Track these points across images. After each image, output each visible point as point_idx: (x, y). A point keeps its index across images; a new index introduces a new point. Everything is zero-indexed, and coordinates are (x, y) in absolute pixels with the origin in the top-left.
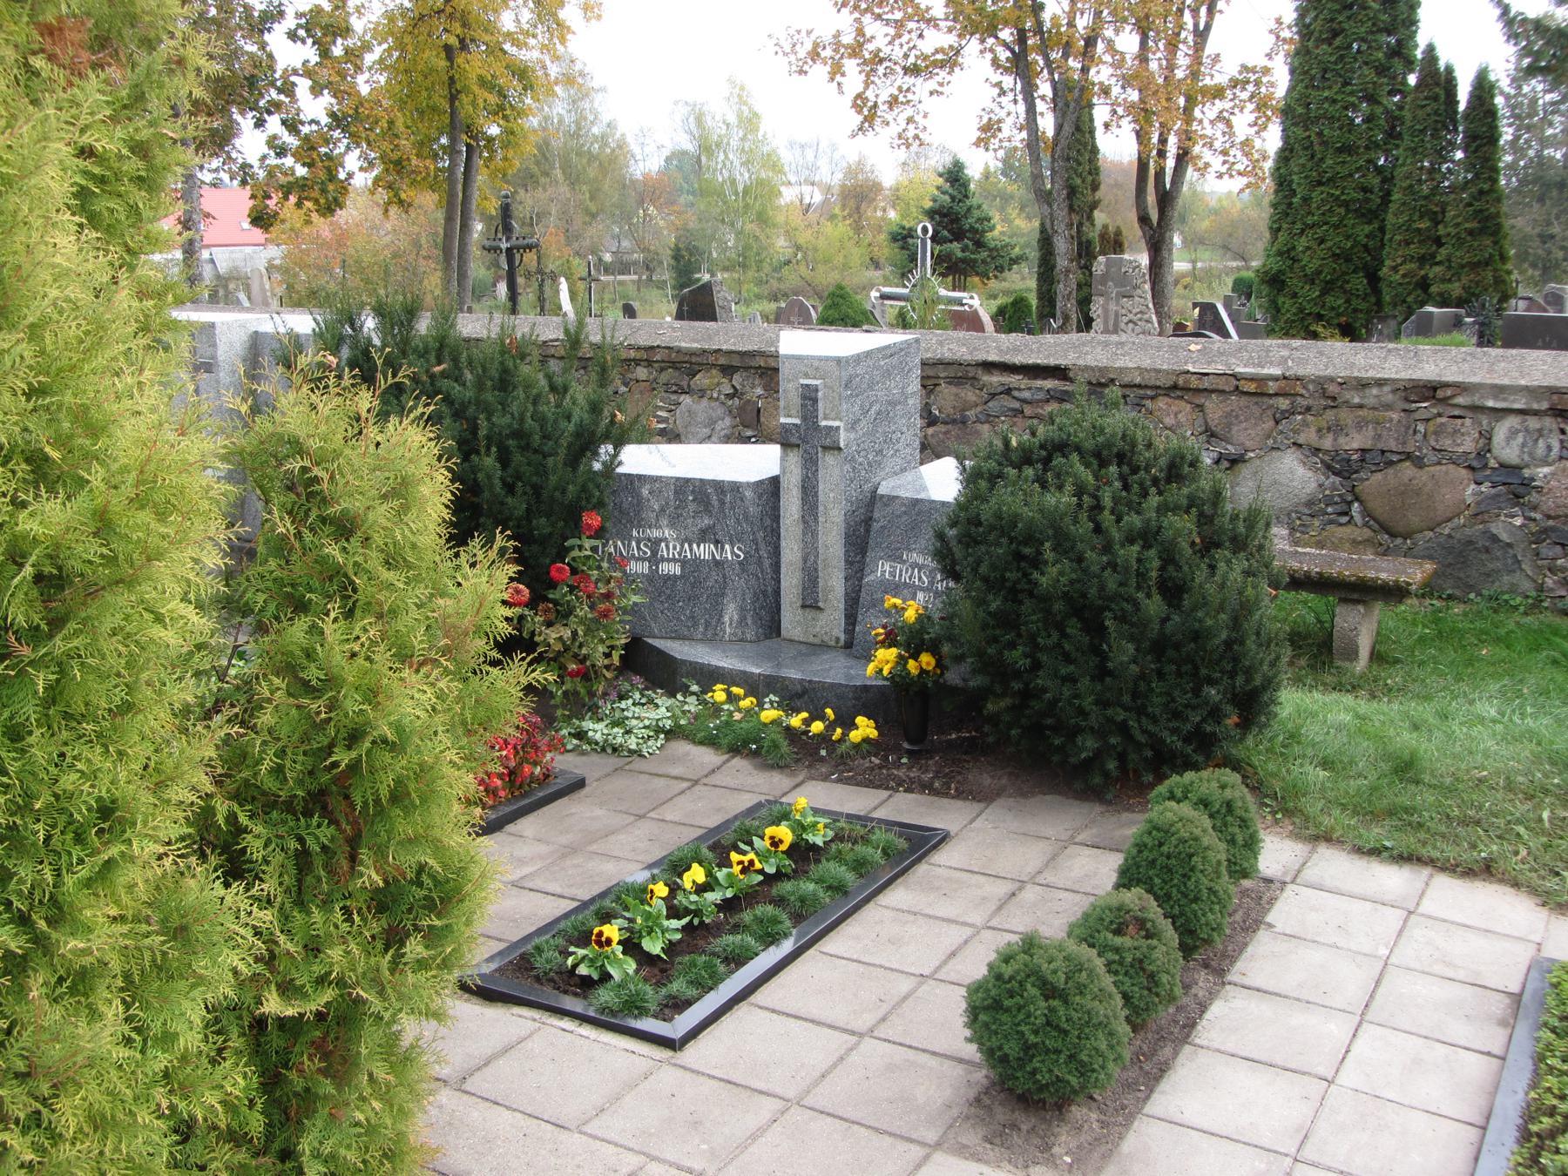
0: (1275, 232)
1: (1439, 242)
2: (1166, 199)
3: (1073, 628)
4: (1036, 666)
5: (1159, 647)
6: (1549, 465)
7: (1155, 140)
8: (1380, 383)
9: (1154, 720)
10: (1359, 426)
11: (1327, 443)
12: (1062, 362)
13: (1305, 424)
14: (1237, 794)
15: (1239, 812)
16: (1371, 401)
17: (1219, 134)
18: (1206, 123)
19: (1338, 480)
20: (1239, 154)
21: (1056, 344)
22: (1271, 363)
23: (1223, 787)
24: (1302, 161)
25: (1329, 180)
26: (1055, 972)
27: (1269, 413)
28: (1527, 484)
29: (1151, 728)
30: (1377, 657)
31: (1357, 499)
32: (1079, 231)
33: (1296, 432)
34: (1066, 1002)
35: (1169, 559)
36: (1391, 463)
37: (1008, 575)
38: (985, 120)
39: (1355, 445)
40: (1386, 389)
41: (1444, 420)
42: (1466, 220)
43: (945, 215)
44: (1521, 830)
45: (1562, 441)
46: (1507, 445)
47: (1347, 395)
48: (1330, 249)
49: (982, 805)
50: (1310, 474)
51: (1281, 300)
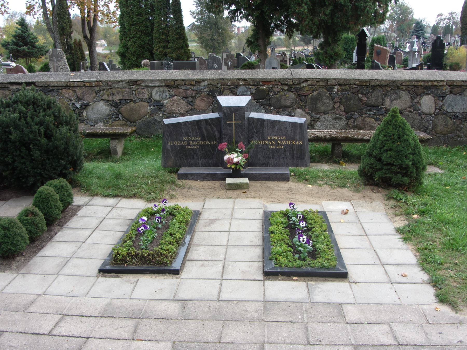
0: (121, 40)
1: (168, 42)
2: (92, 30)
3: (23, 149)
4: (14, 161)
5: (47, 152)
6: (167, 100)
7: (86, 11)
8: (122, 81)
9: (49, 171)
10: (118, 93)
11: (110, 99)
12: (34, 81)
13: (104, 94)
14: (64, 183)
15: (65, 188)
16: (120, 86)
17: (105, 10)
18: (101, 6)
19: (115, 108)
20: (112, 16)
21: (32, 76)
22: (93, 78)
23: (60, 182)
24: (127, 18)
25: (135, 24)
26: (5, 224)
27: (94, 91)
28: (162, 105)
29: (48, 173)
30: (124, 154)
31: (120, 113)
32: (67, 42)
33: (102, 96)
34: (9, 231)
35: (47, 128)
36: (127, 103)
37: (3, 137)
38: (28, 5)
39: (118, 99)
40: (124, 83)
41: (139, 90)
42: (175, 35)
43: (20, 37)
44: (144, 186)
45: (169, 93)
46: (156, 96)
47: (114, 85)
48: (138, 45)
49: (6, 201)
50: (107, 107)
51: (125, 61)
